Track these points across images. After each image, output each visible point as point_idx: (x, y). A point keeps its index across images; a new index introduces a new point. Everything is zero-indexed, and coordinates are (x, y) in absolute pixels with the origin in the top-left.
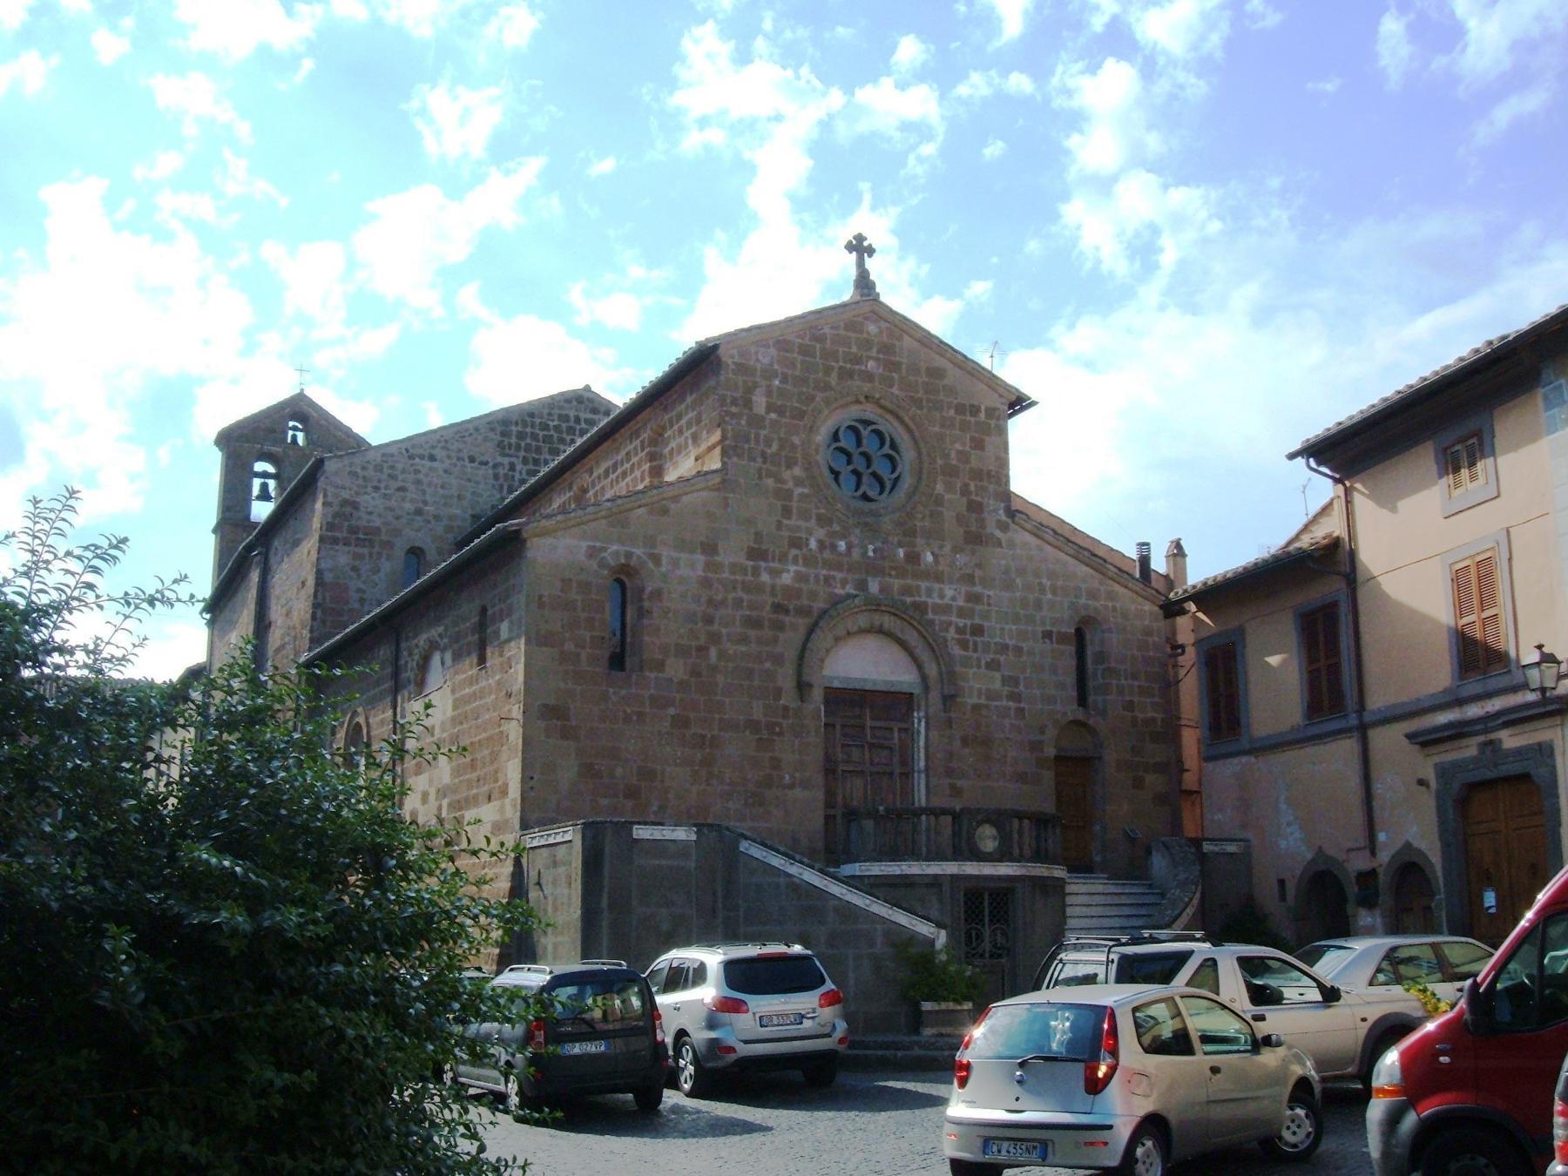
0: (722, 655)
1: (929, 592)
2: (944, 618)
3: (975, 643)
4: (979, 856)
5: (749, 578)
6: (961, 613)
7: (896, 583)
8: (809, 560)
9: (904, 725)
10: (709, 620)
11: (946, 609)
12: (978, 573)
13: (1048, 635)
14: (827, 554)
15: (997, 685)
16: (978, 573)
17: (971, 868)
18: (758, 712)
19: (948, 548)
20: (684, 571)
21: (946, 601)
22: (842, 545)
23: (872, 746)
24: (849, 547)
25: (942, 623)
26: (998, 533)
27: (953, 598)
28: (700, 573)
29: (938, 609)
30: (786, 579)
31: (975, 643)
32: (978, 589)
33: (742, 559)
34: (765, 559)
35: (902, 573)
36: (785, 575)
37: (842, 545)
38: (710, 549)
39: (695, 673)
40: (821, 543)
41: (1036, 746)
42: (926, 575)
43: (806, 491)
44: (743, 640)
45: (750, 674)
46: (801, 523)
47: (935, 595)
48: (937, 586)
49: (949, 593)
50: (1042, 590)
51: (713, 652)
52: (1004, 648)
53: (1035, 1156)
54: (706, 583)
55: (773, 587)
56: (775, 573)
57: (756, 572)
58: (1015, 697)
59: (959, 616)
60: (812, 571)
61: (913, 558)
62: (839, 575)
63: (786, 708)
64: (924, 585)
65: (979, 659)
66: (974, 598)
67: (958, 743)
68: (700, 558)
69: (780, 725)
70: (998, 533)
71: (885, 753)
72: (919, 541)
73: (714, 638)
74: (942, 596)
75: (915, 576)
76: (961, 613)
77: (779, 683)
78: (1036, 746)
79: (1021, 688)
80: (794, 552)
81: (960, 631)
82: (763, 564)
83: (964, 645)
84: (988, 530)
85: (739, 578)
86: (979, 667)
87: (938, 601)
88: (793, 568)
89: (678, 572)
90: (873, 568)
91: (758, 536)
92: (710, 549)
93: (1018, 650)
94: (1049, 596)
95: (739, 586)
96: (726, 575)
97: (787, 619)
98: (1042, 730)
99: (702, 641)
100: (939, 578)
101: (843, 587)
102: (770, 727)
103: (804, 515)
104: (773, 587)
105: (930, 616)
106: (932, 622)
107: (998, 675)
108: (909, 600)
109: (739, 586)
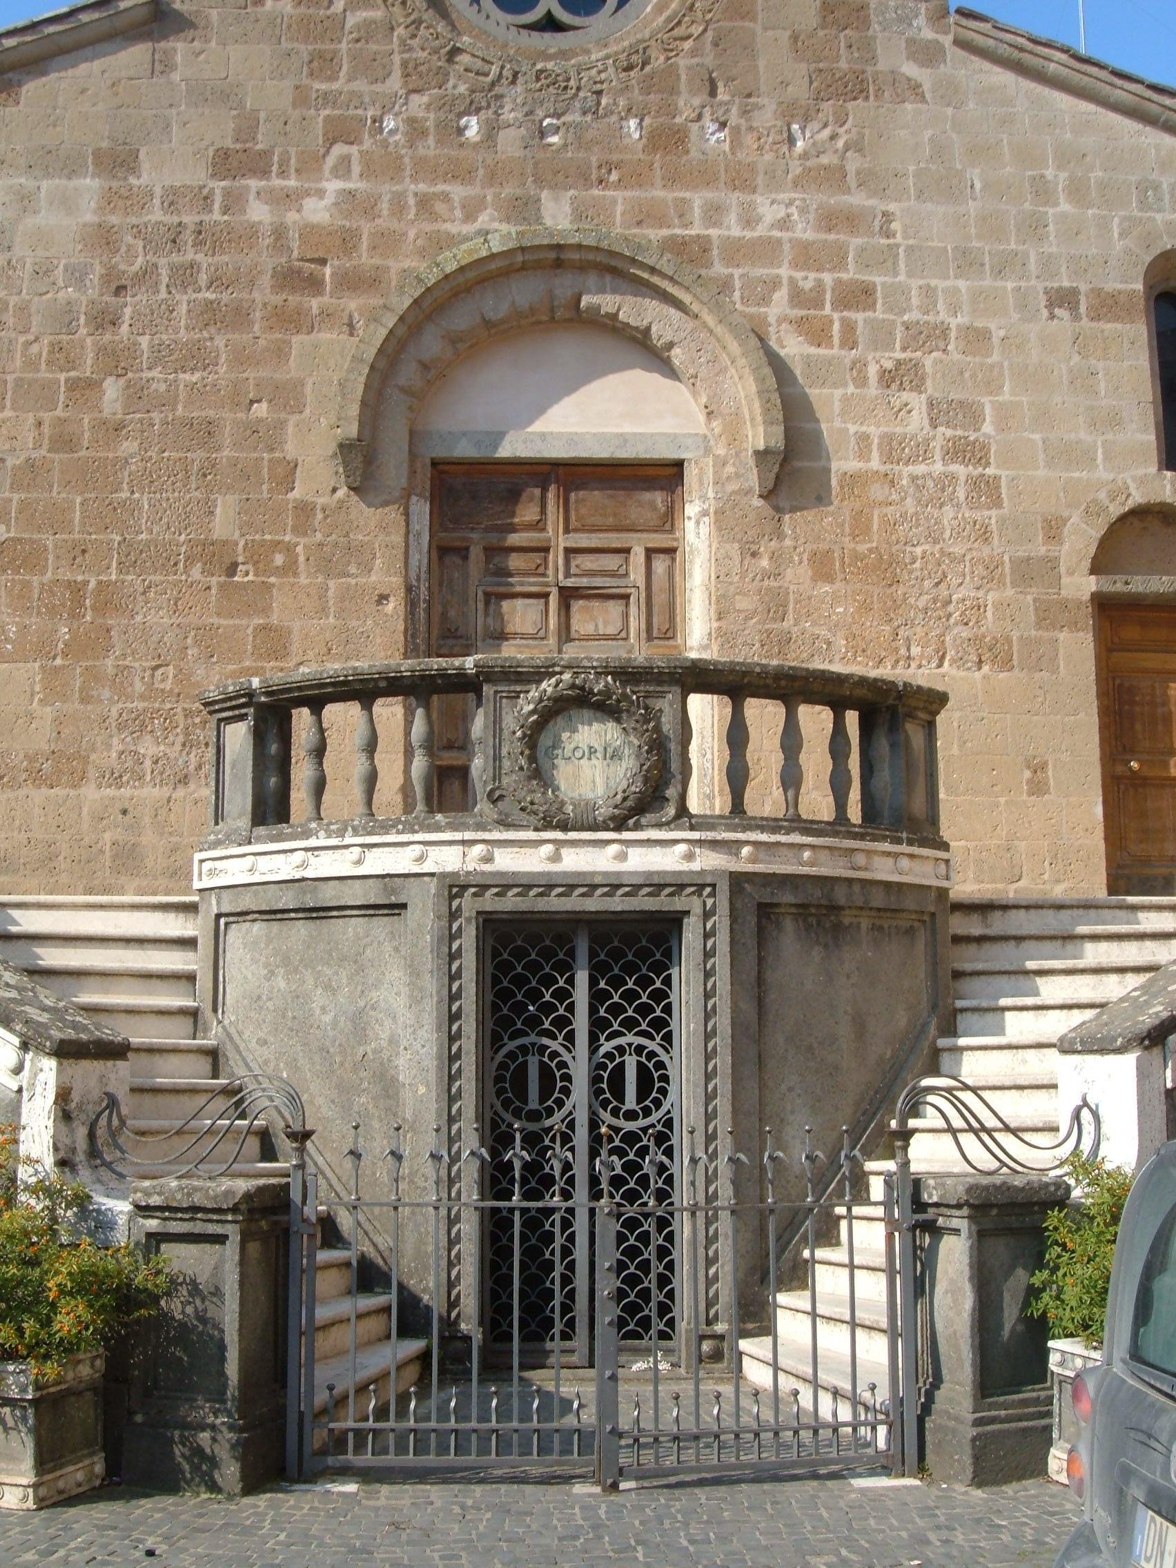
0: (136, 395)
1: (714, 214)
2: (761, 272)
3: (849, 329)
4: (555, 819)
5: (217, 216)
6: (806, 256)
7: (620, 200)
8: (384, 166)
9: (658, 540)
10: (105, 320)
11: (766, 250)
12: (853, 163)
13: (1063, 299)
14: (429, 147)
15: (917, 421)
16: (853, 163)
17: (525, 857)
18: (225, 521)
19: (767, 116)
20: (46, 218)
21: (760, 231)
22: (473, 127)
23: (568, 595)
24: (491, 131)
25: (748, 283)
26: (910, 70)
27: (784, 223)
28: (90, 218)
29: (735, 251)
30: (317, 211)
31: (849, 329)
32: (857, 199)
33: (196, 175)
34: (265, 173)
35: (636, 177)
36: (309, 204)
37: (473, 127)
38: (118, 161)
39: (64, 441)
40: (415, 130)
41: (1030, 572)
42: (705, 176)
43: (378, 14)
44: (197, 357)
45: (209, 429)
46: (360, 85)
47: (732, 218)
48: (734, 198)
49: (769, 211)
50: (1042, 191)
51: (112, 390)
52: (929, 336)
53: (62, 1154)
54: (104, 238)
55: (279, 233)
56: (290, 199)
57: (234, 202)
58: (959, 451)
59: (795, 265)
60: (387, 189)
61: (668, 139)
62: (458, 192)
63: (304, 509)
64: (697, 200)
65: (859, 366)
66: (830, 220)
67: (797, 576)
68: (90, 185)
69: (289, 549)
70: (910, 70)
71: (615, 608)
72: (687, 102)
73: (117, 361)
74: (749, 221)
75: (672, 180)
76: (806, 256)
77: (291, 449)
78: (1030, 572)
79: (988, 428)
80: (339, 150)
81: (797, 297)
82: (254, 184)
83: (817, 334)
84: (882, 66)
85: (189, 219)
86: (862, 381)
87: (736, 232)
88: (333, 186)
89: (30, 221)
90: (554, 174)
91: (248, 127)
92: (118, 161)
93: (977, 338)
94: (1065, 207)
95: (188, 237)
96: (156, 215)
97: (315, 304)
98: (1053, 530)
99: (87, 369)
100: (742, 180)
101: (470, 217)
102: (259, 555)
103: (372, 68)
104: (279, 233)
105: (719, 269)
106: (725, 286)
107: (918, 402)
108: (655, 234)
109: (188, 237)
